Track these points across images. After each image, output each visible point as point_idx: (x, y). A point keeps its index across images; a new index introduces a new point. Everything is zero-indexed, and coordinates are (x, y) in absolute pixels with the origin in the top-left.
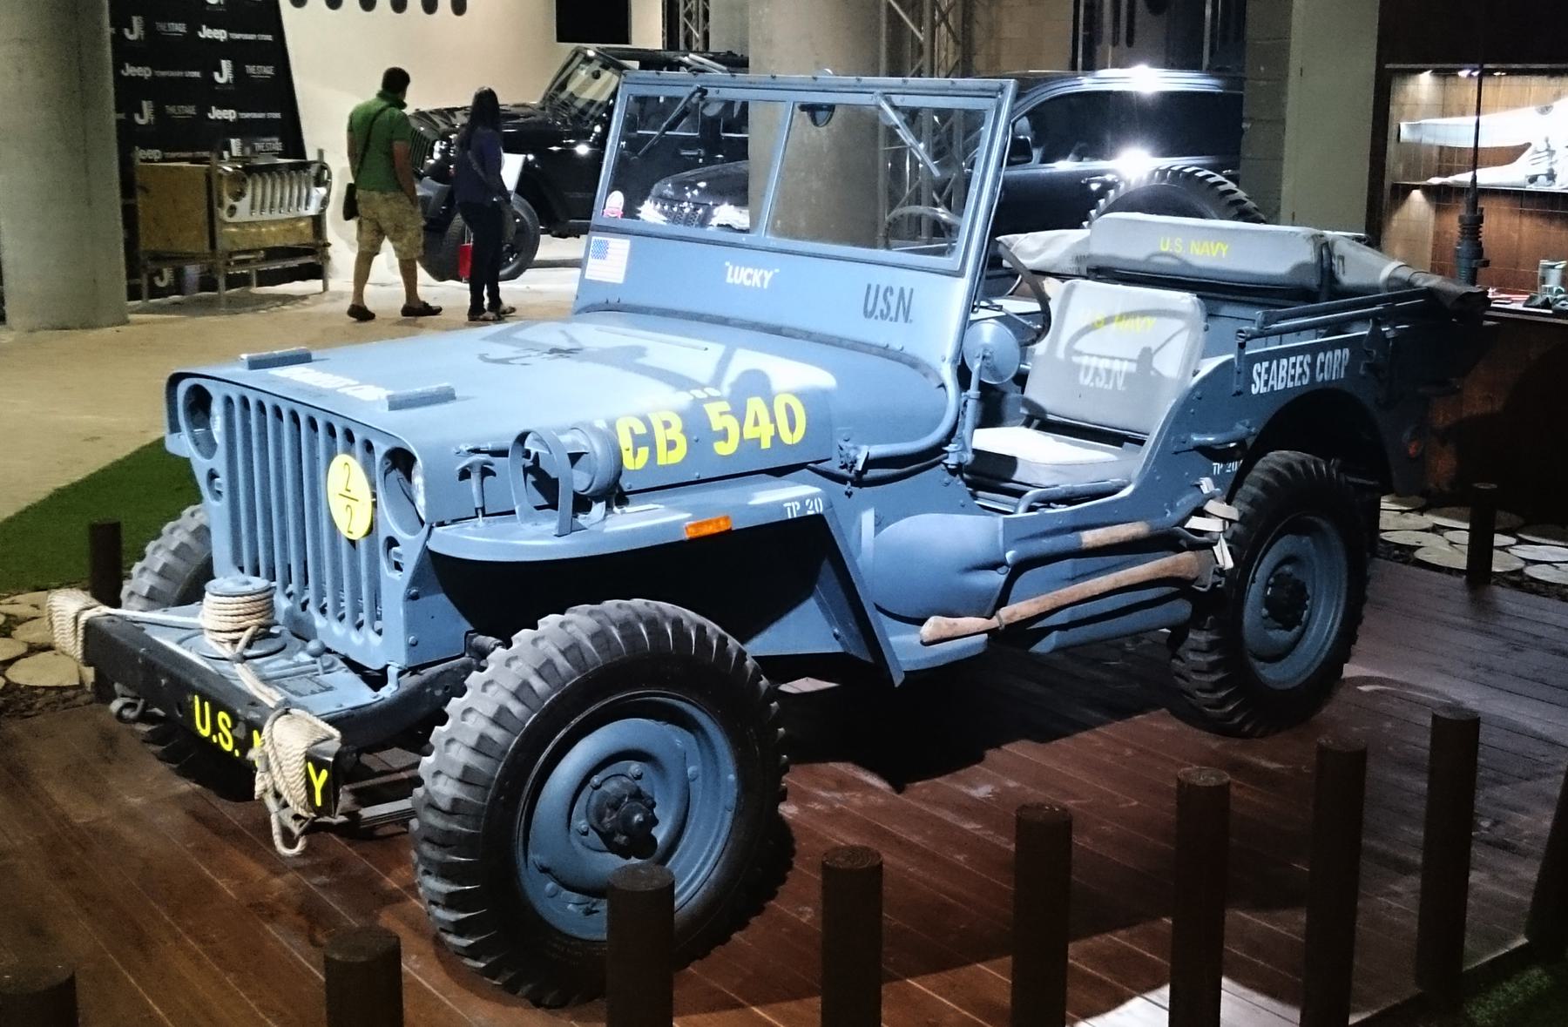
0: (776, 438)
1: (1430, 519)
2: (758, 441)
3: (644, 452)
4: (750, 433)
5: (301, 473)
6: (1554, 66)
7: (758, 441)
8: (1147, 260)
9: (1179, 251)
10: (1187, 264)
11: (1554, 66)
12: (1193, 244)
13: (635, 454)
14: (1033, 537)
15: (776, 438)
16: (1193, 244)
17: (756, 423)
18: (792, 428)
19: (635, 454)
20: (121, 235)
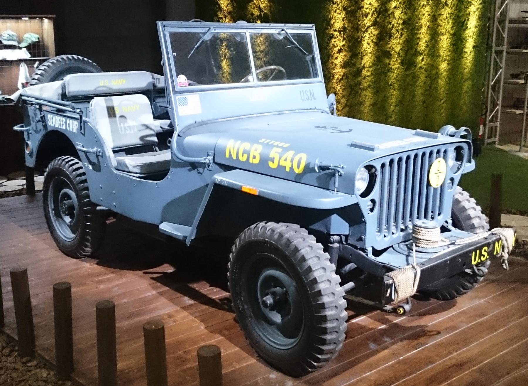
0: (292, 168)
1: (32, 122)
2: (285, 167)
3: (245, 156)
4: (282, 163)
5: (440, 199)
6: (7, 16)
7: (285, 167)
8: (95, 90)
9: (107, 84)
10: (110, 89)
11: (7, 16)
12: (112, 81)
13: (243, 156)
14: (414, 281)
15: (292, 168)
16: (112, 81)
17: (286, 160)
18: (298, 167)
19: (243, 156)
20: (98, 98)
